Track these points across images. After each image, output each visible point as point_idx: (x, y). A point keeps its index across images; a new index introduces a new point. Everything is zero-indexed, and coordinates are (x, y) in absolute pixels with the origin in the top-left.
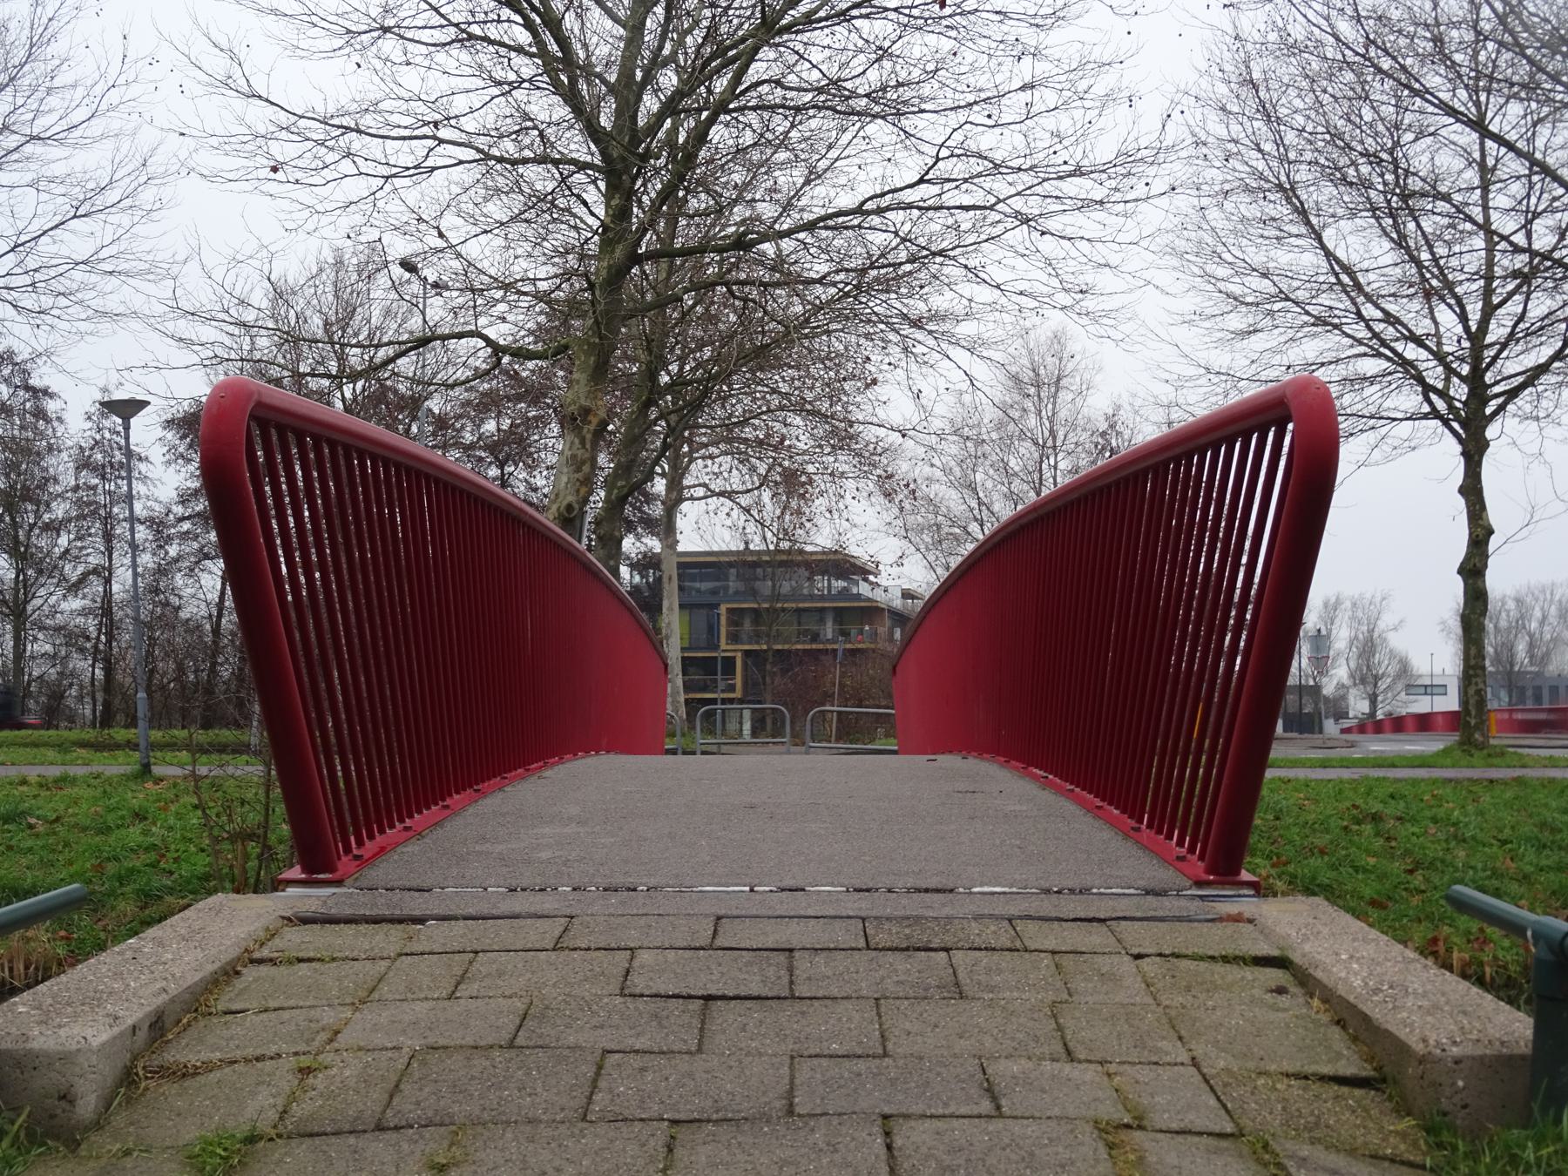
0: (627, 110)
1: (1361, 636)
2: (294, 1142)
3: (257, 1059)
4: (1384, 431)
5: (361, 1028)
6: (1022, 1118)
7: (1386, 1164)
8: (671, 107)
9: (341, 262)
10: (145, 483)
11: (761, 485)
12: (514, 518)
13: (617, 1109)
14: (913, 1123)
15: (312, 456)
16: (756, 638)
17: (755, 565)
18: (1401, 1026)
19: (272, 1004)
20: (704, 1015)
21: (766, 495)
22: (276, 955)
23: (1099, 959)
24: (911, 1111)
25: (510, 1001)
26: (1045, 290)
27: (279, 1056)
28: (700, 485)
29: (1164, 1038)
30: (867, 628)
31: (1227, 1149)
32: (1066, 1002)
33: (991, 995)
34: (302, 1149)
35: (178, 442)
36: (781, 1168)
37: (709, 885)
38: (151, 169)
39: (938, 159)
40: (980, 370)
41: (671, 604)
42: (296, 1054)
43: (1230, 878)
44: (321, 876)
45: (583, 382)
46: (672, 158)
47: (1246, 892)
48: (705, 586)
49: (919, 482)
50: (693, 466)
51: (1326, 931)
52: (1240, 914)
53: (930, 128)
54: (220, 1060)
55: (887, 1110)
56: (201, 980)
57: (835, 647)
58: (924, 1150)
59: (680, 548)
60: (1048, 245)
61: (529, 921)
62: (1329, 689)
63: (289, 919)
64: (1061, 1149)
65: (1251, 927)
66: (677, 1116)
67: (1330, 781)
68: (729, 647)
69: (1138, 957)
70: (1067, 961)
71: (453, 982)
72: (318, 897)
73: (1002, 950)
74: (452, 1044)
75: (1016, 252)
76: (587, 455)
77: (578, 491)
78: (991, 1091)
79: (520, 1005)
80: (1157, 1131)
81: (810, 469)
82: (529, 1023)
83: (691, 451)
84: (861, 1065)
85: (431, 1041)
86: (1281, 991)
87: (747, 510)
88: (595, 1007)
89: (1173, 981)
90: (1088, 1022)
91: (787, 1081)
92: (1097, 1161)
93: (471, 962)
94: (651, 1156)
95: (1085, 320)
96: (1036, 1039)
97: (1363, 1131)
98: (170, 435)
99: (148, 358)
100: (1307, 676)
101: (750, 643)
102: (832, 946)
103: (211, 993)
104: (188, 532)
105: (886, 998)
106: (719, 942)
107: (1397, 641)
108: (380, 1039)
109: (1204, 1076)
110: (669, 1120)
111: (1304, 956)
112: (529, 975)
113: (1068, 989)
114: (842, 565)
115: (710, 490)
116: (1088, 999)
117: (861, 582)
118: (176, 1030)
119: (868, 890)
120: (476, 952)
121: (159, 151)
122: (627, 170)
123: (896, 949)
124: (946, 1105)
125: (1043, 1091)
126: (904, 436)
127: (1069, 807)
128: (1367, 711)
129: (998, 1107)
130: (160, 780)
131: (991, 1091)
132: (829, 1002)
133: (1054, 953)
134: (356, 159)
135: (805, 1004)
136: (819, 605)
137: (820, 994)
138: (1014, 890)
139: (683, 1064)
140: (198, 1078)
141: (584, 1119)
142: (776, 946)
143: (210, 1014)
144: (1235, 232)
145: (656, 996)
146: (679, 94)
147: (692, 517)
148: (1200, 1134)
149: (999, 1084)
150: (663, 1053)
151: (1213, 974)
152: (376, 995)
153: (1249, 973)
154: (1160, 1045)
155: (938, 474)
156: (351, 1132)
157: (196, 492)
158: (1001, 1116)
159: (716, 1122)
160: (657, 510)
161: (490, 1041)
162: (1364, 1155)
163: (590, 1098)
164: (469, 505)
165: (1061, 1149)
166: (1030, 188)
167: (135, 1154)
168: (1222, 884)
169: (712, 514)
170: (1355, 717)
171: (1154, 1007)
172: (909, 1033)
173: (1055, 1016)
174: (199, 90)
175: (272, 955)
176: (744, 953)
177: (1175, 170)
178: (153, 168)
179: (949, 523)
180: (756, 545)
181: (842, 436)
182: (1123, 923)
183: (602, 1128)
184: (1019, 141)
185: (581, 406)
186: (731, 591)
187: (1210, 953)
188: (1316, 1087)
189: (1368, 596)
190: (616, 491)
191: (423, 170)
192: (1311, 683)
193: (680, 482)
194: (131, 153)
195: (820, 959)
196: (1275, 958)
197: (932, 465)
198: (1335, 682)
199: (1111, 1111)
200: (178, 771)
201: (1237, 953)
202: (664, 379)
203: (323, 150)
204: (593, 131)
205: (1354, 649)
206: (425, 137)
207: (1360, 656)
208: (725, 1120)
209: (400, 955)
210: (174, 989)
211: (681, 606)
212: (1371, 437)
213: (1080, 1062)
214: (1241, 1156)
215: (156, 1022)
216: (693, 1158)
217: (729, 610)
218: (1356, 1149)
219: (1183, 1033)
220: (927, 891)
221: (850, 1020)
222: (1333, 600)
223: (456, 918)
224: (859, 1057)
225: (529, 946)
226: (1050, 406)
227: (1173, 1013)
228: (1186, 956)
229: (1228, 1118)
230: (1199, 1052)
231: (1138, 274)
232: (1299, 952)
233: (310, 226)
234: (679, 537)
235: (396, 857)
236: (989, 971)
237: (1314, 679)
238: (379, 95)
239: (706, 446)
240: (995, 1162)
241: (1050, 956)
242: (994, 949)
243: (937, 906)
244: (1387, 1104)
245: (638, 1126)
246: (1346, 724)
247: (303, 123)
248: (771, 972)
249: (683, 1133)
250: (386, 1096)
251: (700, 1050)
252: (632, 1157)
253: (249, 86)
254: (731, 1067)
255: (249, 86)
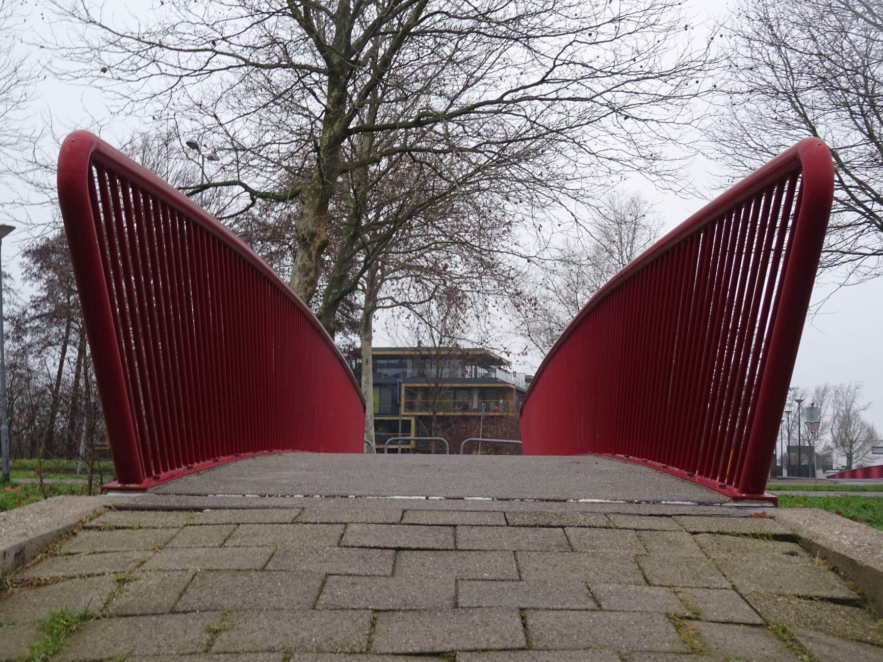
0: (344, 32)
1: (841, 414)
2: (114, 620)
3: (89, 576)
4: (857, 262)
5: (158, 560)
6: (616, 611)
7: (868, 646)
8: (373, 32)
9: (147, 145)
10: (8, 293)
11: (430, 298)
12: (265, 278)
13: (337, 603)
14: (541, 613)
15: (118, 310)
16: (426, 406)
17: (424, 357)
18: (877, 563)
19: (98, 549)
20: (396, 558)
21: (434, 305)
22: (101, 524)
23: (668, 534)
24: (539, 606)
25: (262, 549)
26: (628, 157)
27: (104, 574)
28: (388, 298)
29: (712, 575)
30: (501, 401)
31: (758, 633)
32: (645, 555)
33: (593, 551)
34: (119, 624)
35: (32, 265)
36: (450, 634)
37: (397, 495)
38: (20, 75)
39: (555, 66)
40: (583, 213)
41: (367, 379)
42: (115, 573)
43: (757, 496)
44: (132, 486)
45: (311, 215)
46: (373, 65)
47: (768, 504)
48: (391, 372)
49: (538, 299)
50: (384, 285)
51: (823, 522)
52: (764, 513)
53: (547, 46)
54: (63, 576)
55: (522, 606)
56: (50, 533)
57: (479, 414)
58: (548, 626)
59: (375, 344)
60: (629, 124)
61: (274, 510)
62: (819, 449)
63: (110, 508)
64: (643, 627)
65: (771, 521)
66: (378, 608)
67: (820, 498)
68: (406, 414)
69: (694, 533)
70: (644, 534)
71: (223, 539)
72: (130, 498)
73: (600, 527)
74: (223, 568)
75: (607, 131)
76: (313, 265)
77: (306, 289)
78: (593, 597)
79: (269, 551)
80: (709, 622)
81: (464, 287)
82: (275, 558)
83: (383, 275)
84: (505, 585)
85: (208, 566)
86: (792, 554)
87: (421, 316)
88: (320, 552)
89: (718, 546)
90: (660, 566)
91: (453, 591)
92: (668, 633)
93: (234, 529)
94: (360, 627)
95: (654, 177)
96: (625, 574)
97: (851, 627)
98: (26, 260)
99: (15, 197)
100: (804, 440)
101: (421, 411)
102: (483, 523)
103: (56, 543)
104: (38, 327)
105: (521, 551)
106: (405, 520)
107: (866, 417)
108: (172, 565)
109: (741, 595)
110: (372, 609)
111: (809, 532)
112: (275, 536)
113: (646, 549)
114: (487, 360)
115: (395, 301)
116: (660, 554)
117: (497, 370)
118: (33, 562)
119: (508, 500)
120: (239, 524)
121: (26, 62)
122: (343, 73)
123: (528, 526)
124: (563, 603)
125: (630, 598)
126: (529, 261)
127: (644, 469)
128: (845, 465)
129: (599, 606)
130: (15, 486)
131: (593, 597)
132: (482, 552)
133: (636, 530)
134: (159, 63)
135: (465, 554)
136: (469, 385)
137: (475, 548)
138: (608, 501)
139: (382, 582)
140: (48, 587)
141: (314, 608)
142: (444, 523)
143: (56, 555)
144: (755, 125)
145: (362, 547)
146: (380, 21)
147: (382, 320)
148: (739, 624)
149: (600, 595)
150: (368, 576)
151: (746, 544)
152: (170, 545)
153: (771, 544)
154: (710, 578)
155: (552, 294)
156: (153, 614)
157: (44, 299)
158: (602, 610)
159: (405, 611)
160: (359, 315)
161: (249, 567)
162: (852, 640)
163: (318, 598)
164: (235, 260)
165: (643, 627)
166: (616, 87)
167: (5, 626)
168: (752, 499)
169: (396, 318)
170: (837, 469)
171: (706, 559)
172: (537, 569)
173: (638, 563)
174: (54, 17)
175: (98, 525)
176: (422, 527)
177: (719, 75)
178: (22, 73)
179: (559, 328)
180: (427, 343)
181: (489, 267)
182: (684, 517)
183: (326, 613)
184: (610, 57)
185: (308, 232)
186: (408, 376)
187: (744, 532)
188: (819, 604)
189: (846, 386)
190: (331, 296)
191: (204, 71)
192: (807, 444)
193: (375, 295)
194: (6, 63)
195: (475, 530)
196: (788, 535)
197: (548, 288)
198: (823, 444)
199: (676, 608)
200: (29, 481)
201: (763, 532)
202: (364, 222)
203: (138, 58)
204: (320, 45)
205: (836, 421)
206: (206, 50)
207: (841, 426)
208: (411, 610)
209: (186, 525)
210: (31, 535)
211: (375, 385)
212: (849, 266)
213: (655, 586)
214: (767, 636)
215: (20, 553)
216: (389, 629)
217: (406, 387)
218: (847, 636)
219: (726, 573)
220: (548, 500)
221: (496, 561)
222: (822, 388)
223: (224, 508)
224: (503, 580)
225: (275, 521)
226: (629, 249)
227: (719, 563)
228: (727, 534)
229: (758, 616)
230: (737, 583)
231: (691, 145)
232: (805, 531)
233: (128, 109)
234: (373, 334)
235: (182, 481)
236: (591, 538)
237: (809, 442)
238: (175, 20)
239: (393, 271)
240: (597, 632)
241: (633, 531)
242: (595, 527)
243: (556, 507)
244: (868, 615)
245: (350, 613)
246: (831, 473)
247: (123, 40)
248: (442, 537)
249: (381, 617)
250: (177, 595)
251: (393, 575)
252: (347, 628)
253: (88, 15)
254: (414, 584)
255: (88, 15)
